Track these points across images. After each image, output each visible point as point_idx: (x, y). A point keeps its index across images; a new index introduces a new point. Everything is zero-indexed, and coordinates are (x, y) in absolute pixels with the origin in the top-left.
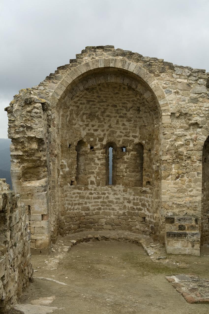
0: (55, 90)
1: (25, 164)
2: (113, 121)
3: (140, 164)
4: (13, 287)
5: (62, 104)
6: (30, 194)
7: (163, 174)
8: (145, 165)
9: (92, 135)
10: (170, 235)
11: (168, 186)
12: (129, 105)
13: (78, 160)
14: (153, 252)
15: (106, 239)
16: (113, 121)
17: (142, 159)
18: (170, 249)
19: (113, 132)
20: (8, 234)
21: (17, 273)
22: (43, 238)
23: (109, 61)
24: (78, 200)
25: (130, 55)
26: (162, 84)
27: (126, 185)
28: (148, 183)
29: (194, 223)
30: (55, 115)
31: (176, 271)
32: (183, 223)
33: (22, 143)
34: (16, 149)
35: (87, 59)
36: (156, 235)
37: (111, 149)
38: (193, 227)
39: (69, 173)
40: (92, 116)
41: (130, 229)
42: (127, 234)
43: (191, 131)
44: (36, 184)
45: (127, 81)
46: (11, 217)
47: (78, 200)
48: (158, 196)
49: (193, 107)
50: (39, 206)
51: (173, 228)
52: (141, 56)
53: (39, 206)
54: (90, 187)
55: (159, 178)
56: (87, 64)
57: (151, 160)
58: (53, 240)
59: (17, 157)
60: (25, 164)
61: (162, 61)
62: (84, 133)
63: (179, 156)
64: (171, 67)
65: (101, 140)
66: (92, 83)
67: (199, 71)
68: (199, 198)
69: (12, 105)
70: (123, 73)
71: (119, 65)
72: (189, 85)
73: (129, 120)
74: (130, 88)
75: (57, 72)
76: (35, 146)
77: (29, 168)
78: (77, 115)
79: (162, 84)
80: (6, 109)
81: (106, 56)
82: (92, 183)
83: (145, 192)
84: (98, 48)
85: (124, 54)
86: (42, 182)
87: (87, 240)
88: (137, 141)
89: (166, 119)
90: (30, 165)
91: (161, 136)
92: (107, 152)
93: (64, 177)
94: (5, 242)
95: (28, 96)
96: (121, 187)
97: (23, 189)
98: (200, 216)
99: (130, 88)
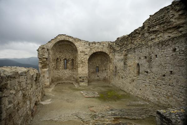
0: (50, 45)
1: (43, 65)
2: (66, 53)
3: (73, 64)
4: (39, 98)
5: (52, 49)
6: (44, 72)
7: (79, 66)
8: (74, 64)
9: (61, 57)
10: (80, 81)
11: (80, 69)
12: (70, 49)
13: (57, 63)
14: (76, 86)
15: (64, 83)
16: (66, 53)
17: (73, 63)
18: (80, 85)
19: (66, 56)
20: (38, 84)
21: (41, 94)
22: (48, 84)
23: (65, 38)
24: (57, 73)
25: (70, 37)
26: (78, 44)
27: (69, 69)
28: (75, 69)
29: (86, 78)
30: (50, 52)
31: (82, 90)
32: (83, 78)
33: (42, 59)
34: (40, 61)
35: (59, 37)
36: (77, 81)
37: (65, 60)
38: (86, 79)
39: (55, 67)
40: (60, 52)
41: (70, 80)
42: (70, 81)
43: (85, 56)
44: (46, 70)
45: (69, 43)
46: (39, 79)
47: (57, 73)
48: (77, 72)
49: (86, 50)
50: (47, 75)
51: (81, 80)
52: (73, 37)
53: (47, 75)
54: (60, 70)
55: (78, 68)
56: (59, 39)
57: (76, 63)
58: (50, 84)
59: (40, 63)
60: (43, 65)
61: (78, 39)
62: (58, 56)
63: (82, 62)
64: (80, 40)
65: (63, 58)
66: (60, 44)
67: (87, 41)
68: (87, 72)
69: (39, 49)
70: (68, 41)
71: (67, 39)
72: (85, 45)
73: (70, 53)
74: (70, 45)
75: (51, 41)
76: (45, 60)
77: (44, 66)
78: (57, 51)
79: (78, 44)
80: (37, 50)
81: (64, 37)
82: (61, 69)
83: (74, 71)
84: (62, 35)
85: (68, 36)
86: (47, 69)
87: (60, 83)
88: (72, 58)
89: (79, 53)
90: (44, 65)
91: (78, 57)
92: (64, 61)
93: (53, 68)
94: (37, 86)
95: (43, 47)
96: (68, 70)
97: (42, 71)
98: (87, 76)
99: (70, 45)
